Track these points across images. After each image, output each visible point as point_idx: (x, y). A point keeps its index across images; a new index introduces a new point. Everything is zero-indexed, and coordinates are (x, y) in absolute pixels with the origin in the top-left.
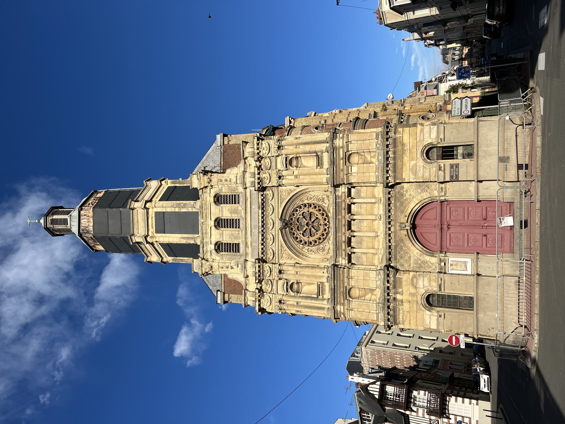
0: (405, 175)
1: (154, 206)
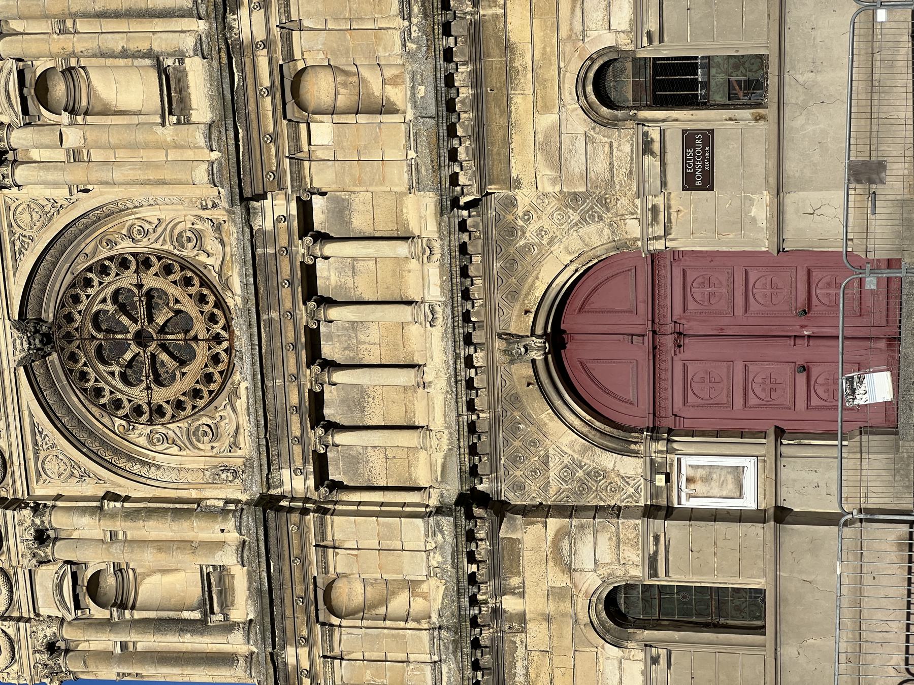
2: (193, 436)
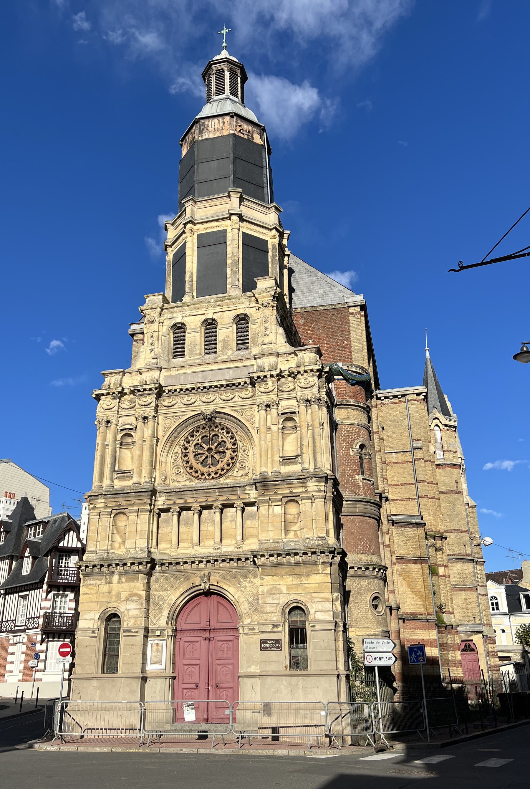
0: (267, 579)
1: (234, 227)
2: (178, 467)
